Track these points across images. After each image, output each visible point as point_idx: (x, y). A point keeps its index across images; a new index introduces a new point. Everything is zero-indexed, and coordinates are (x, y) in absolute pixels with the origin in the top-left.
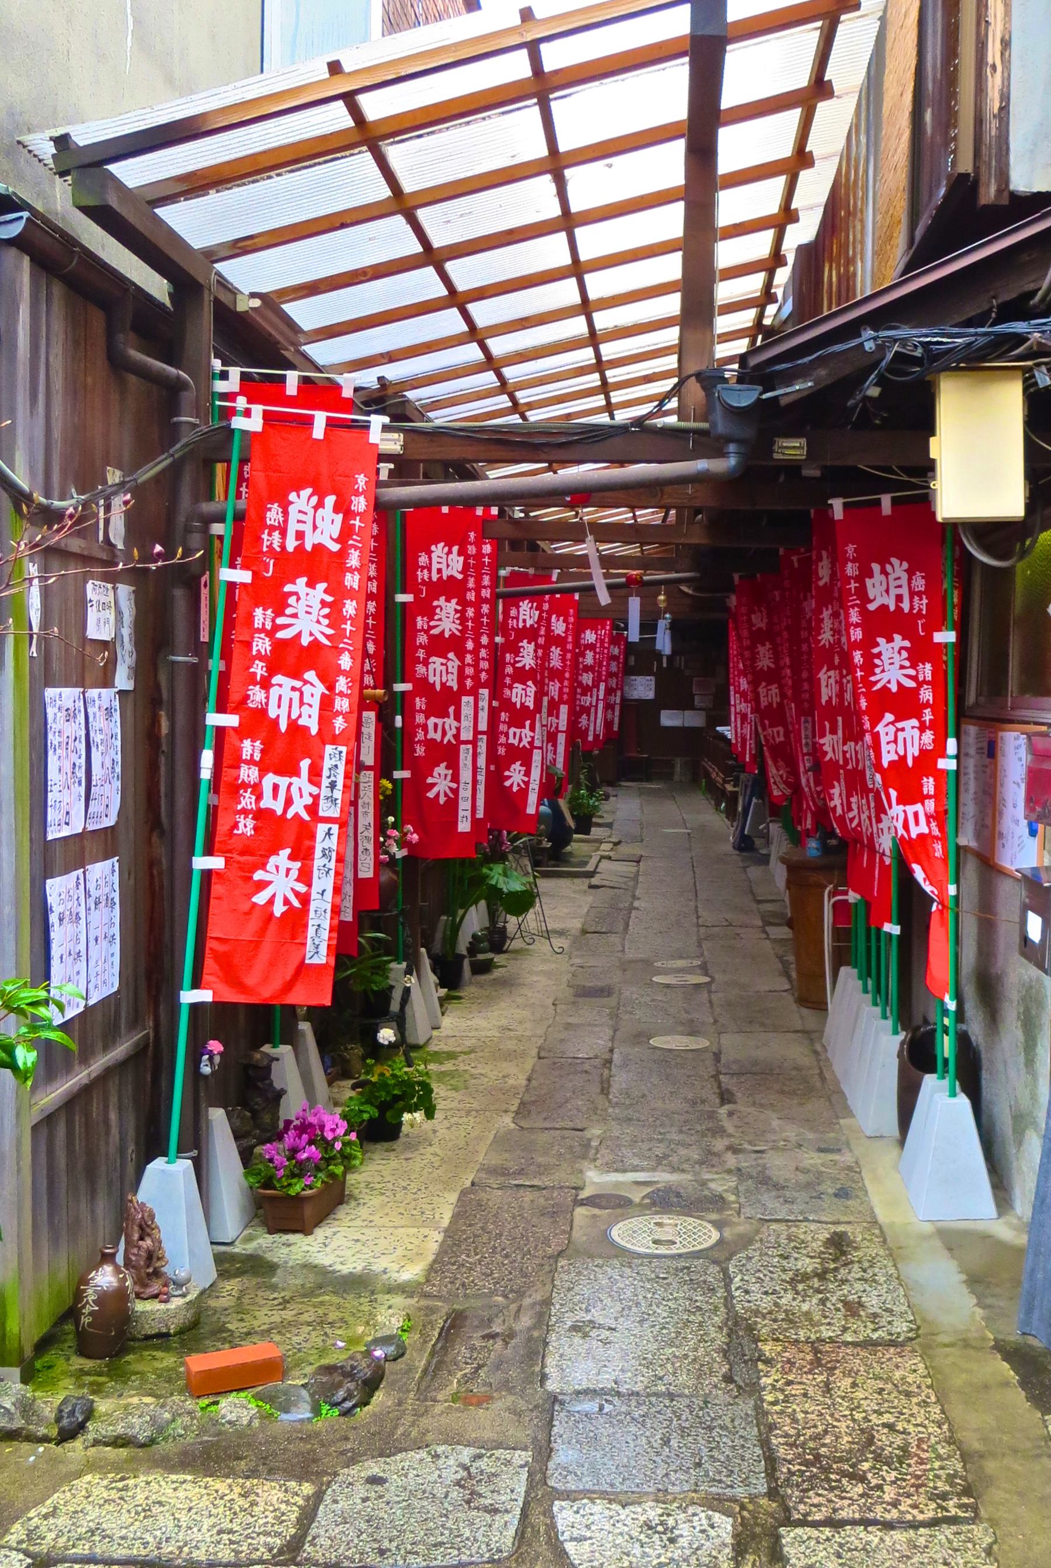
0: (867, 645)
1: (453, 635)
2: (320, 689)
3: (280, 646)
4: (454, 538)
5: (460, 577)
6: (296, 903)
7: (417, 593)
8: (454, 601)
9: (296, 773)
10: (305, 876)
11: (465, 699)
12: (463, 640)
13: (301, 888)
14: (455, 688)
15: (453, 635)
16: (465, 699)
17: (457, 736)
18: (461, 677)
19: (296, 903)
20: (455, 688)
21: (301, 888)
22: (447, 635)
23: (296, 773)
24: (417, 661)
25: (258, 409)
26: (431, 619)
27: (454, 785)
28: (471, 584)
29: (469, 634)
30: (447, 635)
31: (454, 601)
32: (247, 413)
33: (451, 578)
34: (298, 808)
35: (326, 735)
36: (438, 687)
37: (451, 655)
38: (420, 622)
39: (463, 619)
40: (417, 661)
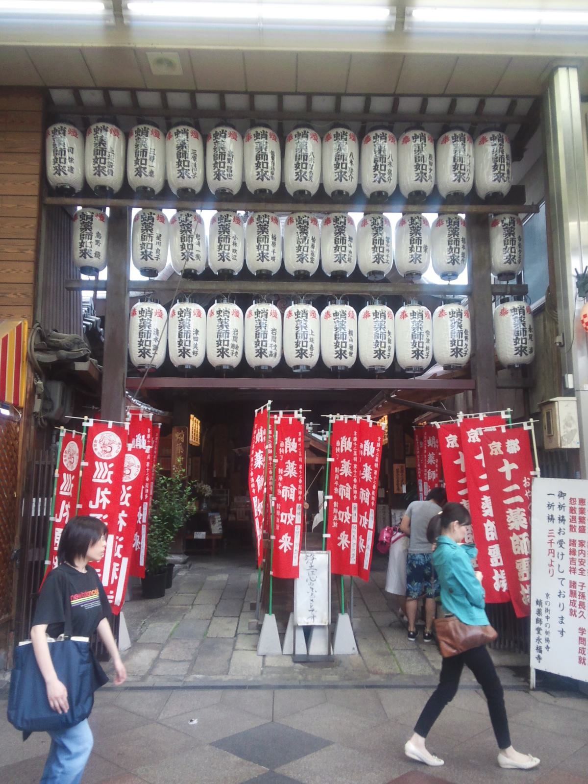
0: (427, 454)
1: (348, 476)
2: (295, 489)
3: (284, 478)
4: (349, 435)
5: (296, 451)
6: (290, 548)
7: (335, 457)
8: (294, 462)
9: (289, 512)
10: (292, 541)
11: (298, 505)
12: (353, 478)
13: (349, 542)
14: (293, 500)
15: (348, 476)
16: (298, 505)
17: (350, 520)
18: (297, 495)
19: (290, 548)
20: (293, 500)
21: (349, 542)
22: (346, 475)
23: (289, 512)
24: (335, 486)
25: (92, 420)
26: (284, 470)
27: (291, 544)
28: (355, 454)
29: (300, 476)
30: (346, 475)
31: (294, 462)
32: (88, 421)
33: (293, 452)
34: (290, 522)
35: (297, 501)
36: (286, 500)
37: (347, 484)
38: (337, 469)
39: (352, 469)
40: (335, 486)
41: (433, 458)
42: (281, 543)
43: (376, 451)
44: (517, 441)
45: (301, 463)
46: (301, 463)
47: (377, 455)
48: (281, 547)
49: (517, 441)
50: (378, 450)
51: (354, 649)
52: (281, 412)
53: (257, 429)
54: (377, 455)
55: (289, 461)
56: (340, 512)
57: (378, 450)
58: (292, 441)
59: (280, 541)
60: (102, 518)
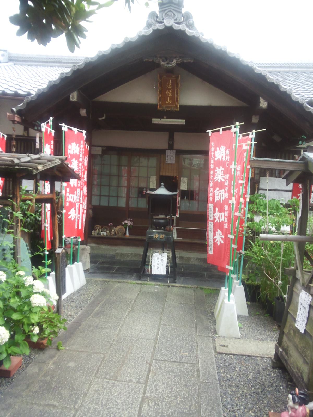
23: (74, 194)
41: (221, 173)
42: (70, 215)
43: (80, 151)
44: (258, 117)
45: (80, 162)
46: (80, 162)
47: (81, 152)
48: (69, 217)
49: (258, 117)
50: (81, 150)
51: (38, 289)
52: (221, 129)
53: (214, 152)
54: (81, 152)
55: (74, 159)
56: (71, 195)
57: (81, 150)
58: (76, 146)
59: (69, 213)
60: (234, 272)
